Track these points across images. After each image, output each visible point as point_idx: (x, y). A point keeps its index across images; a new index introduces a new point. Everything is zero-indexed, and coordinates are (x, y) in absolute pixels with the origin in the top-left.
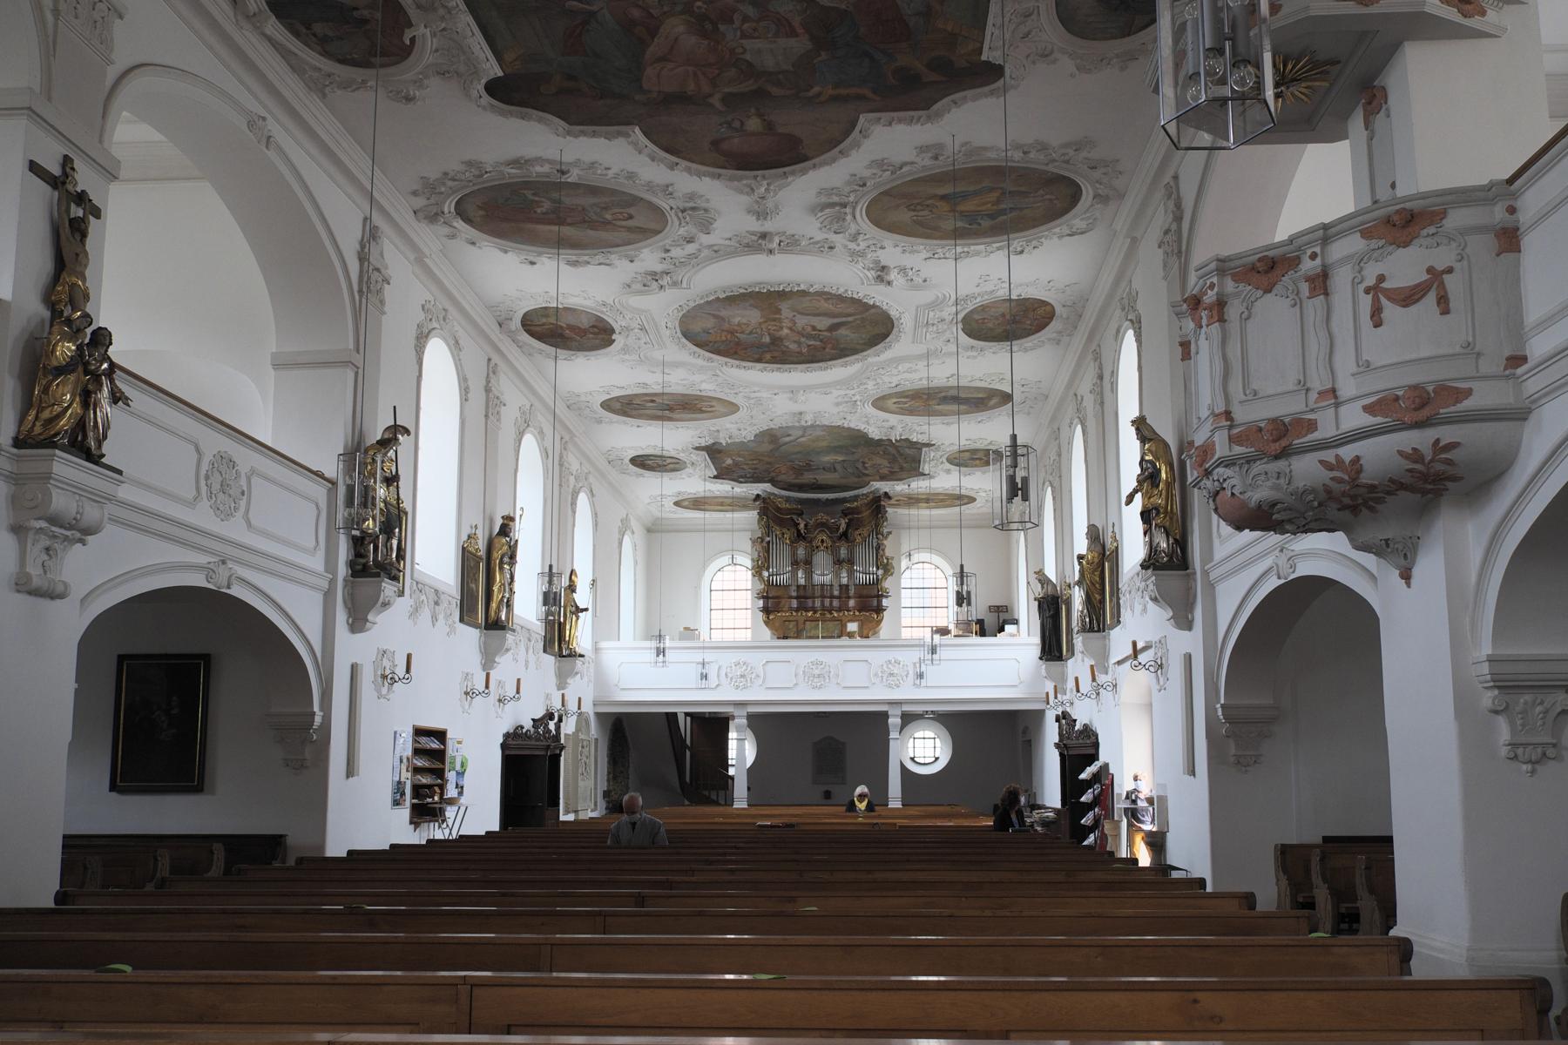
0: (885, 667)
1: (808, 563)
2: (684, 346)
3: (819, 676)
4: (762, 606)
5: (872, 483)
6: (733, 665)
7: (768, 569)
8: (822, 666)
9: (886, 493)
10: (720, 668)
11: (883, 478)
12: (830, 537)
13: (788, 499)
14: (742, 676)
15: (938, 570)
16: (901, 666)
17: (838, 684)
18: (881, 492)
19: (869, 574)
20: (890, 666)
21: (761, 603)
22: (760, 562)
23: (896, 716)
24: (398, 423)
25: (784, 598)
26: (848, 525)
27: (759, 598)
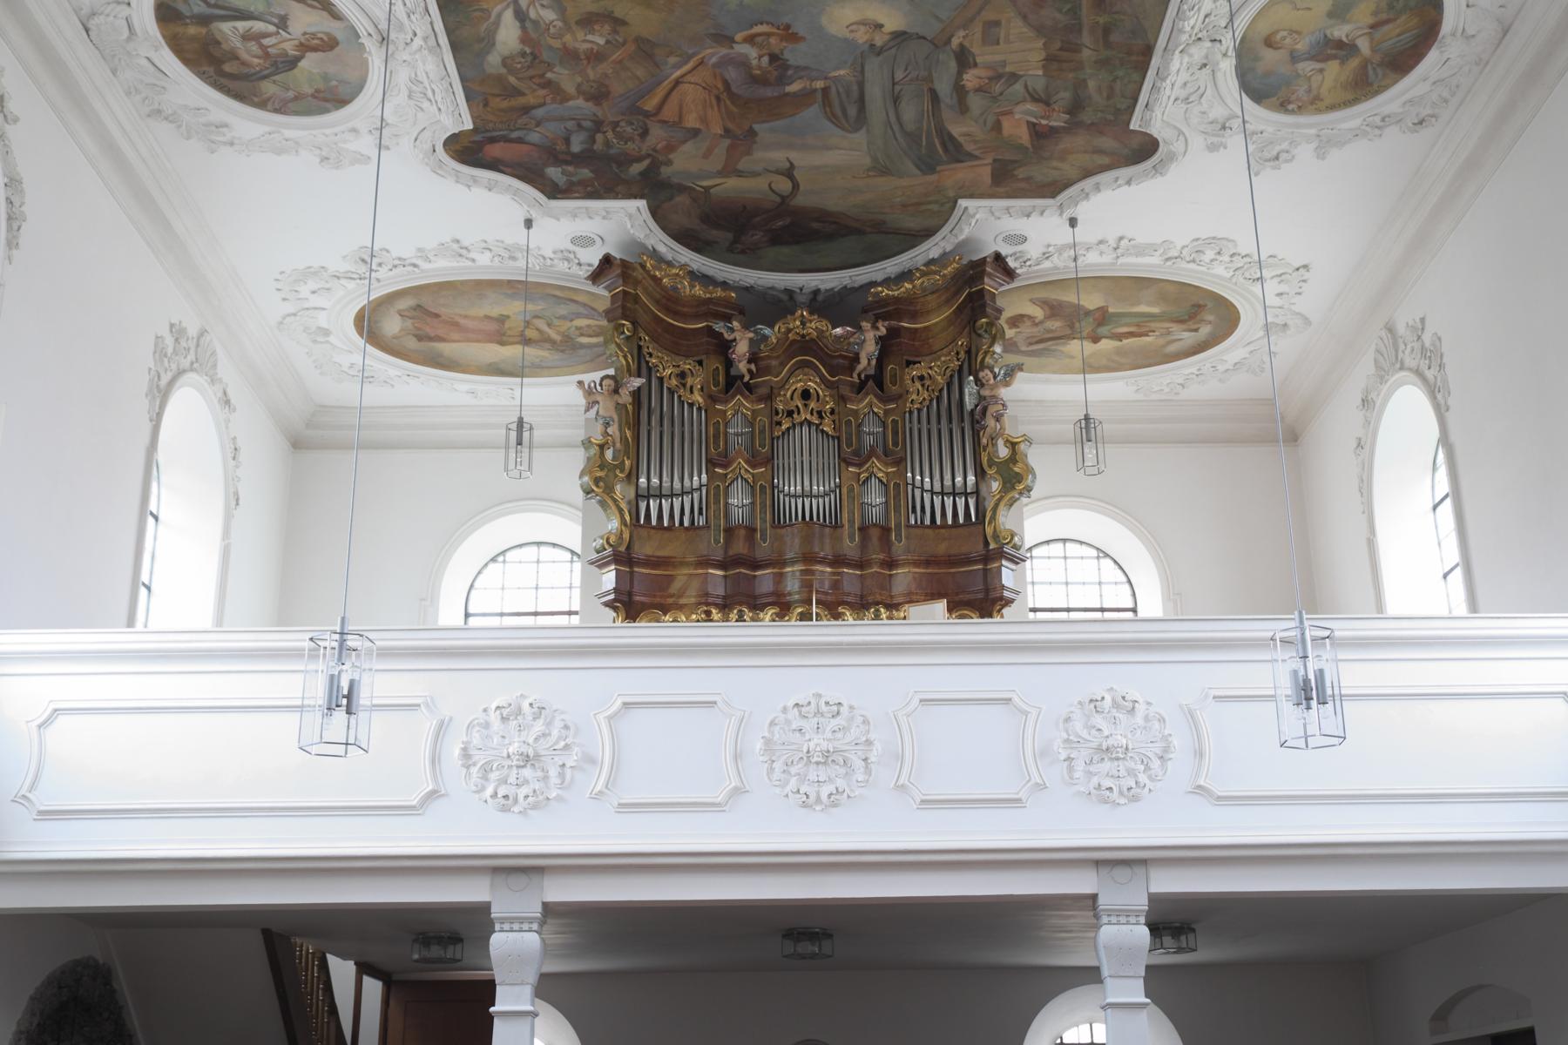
0: (1078, 725)
1: (764, 458)
2: (475, 180)
3: (828, 758)
6: (494, 718)
7: (632, 476)
8: (838, 721)
9: (998, 258)
10: (441, 728)
12: (829, 385)
13: (696, 277)
14: (527, 760)
15: (1107, 563)
16: (1139, 719)
17: (901, 788)
18: (988, 251)
19: (966, 494)
20: (1098, 720)
21: (609, 579)
22: (609, 454)
23: (1123, 914)
25: (683, 564)
27: (601, 564)
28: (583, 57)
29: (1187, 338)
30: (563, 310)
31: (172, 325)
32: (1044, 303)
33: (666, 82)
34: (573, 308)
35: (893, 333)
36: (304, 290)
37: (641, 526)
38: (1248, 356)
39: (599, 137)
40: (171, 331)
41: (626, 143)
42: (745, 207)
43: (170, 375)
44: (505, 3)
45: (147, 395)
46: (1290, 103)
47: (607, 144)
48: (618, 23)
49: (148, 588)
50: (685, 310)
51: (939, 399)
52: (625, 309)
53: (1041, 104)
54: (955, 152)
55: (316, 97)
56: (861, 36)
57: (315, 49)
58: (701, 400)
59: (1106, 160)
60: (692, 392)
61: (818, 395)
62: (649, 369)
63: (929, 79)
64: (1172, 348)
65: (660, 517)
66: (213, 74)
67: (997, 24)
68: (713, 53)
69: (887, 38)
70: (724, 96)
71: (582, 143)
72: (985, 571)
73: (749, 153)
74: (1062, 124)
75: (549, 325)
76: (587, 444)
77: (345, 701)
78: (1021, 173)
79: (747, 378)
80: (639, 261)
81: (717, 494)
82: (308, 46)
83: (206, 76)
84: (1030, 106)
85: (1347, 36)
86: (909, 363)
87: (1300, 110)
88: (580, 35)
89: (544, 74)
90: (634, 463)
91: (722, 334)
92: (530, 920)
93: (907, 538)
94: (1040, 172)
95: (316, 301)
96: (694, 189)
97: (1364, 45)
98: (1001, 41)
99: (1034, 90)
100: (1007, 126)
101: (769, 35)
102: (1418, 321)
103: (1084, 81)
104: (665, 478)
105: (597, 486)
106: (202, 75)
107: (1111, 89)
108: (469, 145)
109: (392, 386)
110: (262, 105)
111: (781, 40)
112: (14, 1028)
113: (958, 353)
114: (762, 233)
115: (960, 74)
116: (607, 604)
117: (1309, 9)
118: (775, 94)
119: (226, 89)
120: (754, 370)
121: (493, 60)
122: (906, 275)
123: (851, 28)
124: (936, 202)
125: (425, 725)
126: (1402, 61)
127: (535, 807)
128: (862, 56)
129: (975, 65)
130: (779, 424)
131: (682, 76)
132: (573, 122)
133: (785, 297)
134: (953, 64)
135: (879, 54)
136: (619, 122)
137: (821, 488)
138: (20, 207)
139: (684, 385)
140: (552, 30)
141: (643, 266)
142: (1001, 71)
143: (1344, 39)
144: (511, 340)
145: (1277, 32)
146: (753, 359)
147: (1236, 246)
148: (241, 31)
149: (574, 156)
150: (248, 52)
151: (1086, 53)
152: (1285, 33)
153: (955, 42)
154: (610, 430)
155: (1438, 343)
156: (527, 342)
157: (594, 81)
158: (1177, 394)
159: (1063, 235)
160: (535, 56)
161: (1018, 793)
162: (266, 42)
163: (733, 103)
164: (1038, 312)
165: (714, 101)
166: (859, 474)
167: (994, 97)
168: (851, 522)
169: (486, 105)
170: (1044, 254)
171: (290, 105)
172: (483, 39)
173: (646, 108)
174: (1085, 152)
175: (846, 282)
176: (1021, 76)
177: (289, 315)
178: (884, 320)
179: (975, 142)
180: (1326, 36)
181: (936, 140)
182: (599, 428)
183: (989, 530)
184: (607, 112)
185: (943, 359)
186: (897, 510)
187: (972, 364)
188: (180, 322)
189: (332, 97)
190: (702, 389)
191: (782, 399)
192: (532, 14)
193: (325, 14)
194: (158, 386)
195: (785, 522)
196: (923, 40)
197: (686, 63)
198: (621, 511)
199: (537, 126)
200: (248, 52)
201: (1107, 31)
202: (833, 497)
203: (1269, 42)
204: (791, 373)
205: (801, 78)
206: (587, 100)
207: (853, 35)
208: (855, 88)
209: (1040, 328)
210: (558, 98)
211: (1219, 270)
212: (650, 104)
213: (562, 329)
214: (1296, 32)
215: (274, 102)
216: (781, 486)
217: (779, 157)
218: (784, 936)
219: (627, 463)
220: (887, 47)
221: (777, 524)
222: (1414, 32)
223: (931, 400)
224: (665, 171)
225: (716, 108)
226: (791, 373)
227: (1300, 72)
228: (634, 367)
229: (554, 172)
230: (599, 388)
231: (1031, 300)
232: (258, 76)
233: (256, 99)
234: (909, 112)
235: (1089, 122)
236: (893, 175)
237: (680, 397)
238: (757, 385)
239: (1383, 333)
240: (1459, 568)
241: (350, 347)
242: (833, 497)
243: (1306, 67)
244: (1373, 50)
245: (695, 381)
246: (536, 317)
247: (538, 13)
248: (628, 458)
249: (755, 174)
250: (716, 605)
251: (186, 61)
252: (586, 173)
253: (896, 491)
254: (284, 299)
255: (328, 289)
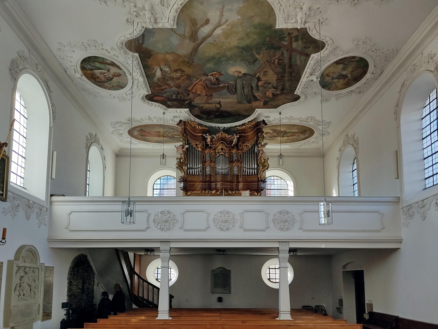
1: (213, 161)
4: (183, 186)
5: (256, 110)
11: (266, 105)
13: (199, 124)
14: (166, 221)
19: (255, 169)
21: (182, 185)
22: (182, 160)
24: (158, 278)
26: (239, 139)
27: (180, 182)
28: (175, 78)
29: (303, 137)
30: (171, 131)
31: (89, 133)
32: (273, 130)
33: (193, 84)
34: (174, 130)
35: (240, 136)
36: (117, 126)
37: (188, 175)
38: (315, 140)
39: (179, 96)
40: (89, 135)
41: (185, 97)
42: (210, 110)
43: (90, 144)
44: (158, 67)
45: (85, 148)
46: (331, 88)
47: (181, 97)
48: (183, 71)
49: (89, 185)
50: (197, 131)
51: (250, 150)
52: (185, 132)
53: (275, 89)
54: (256, 99)
55: (117, 87)
56: (236, 74)
57: (116, 76)
58: (200, 150)
59: (288, 101)
60: (199, 148)
61: (225, 149)
62: (190, 144)
63: (251, 84)
64: (299, 139)
65: (192, 173)
66: (94, 81)
67: (267, 71)
68: (204, 78)
69: (242, 75)
70: (206, 87)
71: (175, 97)
72: (258, 184)
73: (211, 99)
74: (280, 93)
75: (169, 133)
76: (177, 159)
77: (130, 214)
78: (270, 103)
79: (210, 146)
80: (187, 121)
81: (204, 168)
82: (114, 76)
83: (93, 81)
84: (273, 89)
85: (346, 74)
86: (244, 143)
87: (333, 90)
88: (174, 74)
89: (166, 82)
90: (187, 162)
91: (205, 137)
92: (168, 251)
93: (242, 177)
94: (273, 103)
95: (119, 128)
96: (199, 107)
97: (349, 76)
98: (267, 75)
99: (274, 86)
100: (267, 93)
101: (216, 74)
102: (354, 134)
103: (285, 84)
104: (193, 165)
105: (179, 167)
106: (92, 82)
107: (291, 85)
108: (151, 97)
109: (136, 145)
110: (105, 88)
111: (219, 75)
112: (69, 267)
113: (254, 141)
114: (213, 116)
115: (258, 82)
116: (181, 190)
117: (338, 68)
118: (217, 87)
119: (97, 85)
120: (211, 144)
121: (155, 79)
122: (244, 124)
123: (234, 73)
124: (251, 109)
125: (145, 215)
126: (357, 79)
127: (168, 230)
128: (236, 79)
129: (261, 81)
130: (217, 155)
131: (197, 83)
132: (173, 92)
133: (218, 128)
134: (256, 81)
135: (240, 78)
136: (183, 92)
137: (225, 167)
138: (55, 111)
139: (197, 147)
140: (168, 73)
141: (188, 122)
142: (267, 82)
143: (345, 74)
144: (161, 136)
145: (329, 73)
146: (211, 141)
147: (315, 118)
148: (100, 72)
149: (173, 99)
150: (102, 76)
151: (286, 78)
152: (331, 73)
153: (257, 76)
154: (182, 156)
155: (358, 139)
156: (164, 137)
157: (177, 84)
158: (299, 147)
159: (277, 116)
160: (164, 78)
161: (264, 229)
162: (105, 74)
163: (208, 89)
164: (271, 132)
165: (204, 88)
166: (233, 165)
167: (265, 88)
168: (231, 174)
169: (154, 89)
170: (273, 120)
171: (111, 88)
172: (153, 75)
173: (189, 90)
174: (284, 99)
175: (231, 126)
176: (271, 83)
177: (114, 131)
178: (239, 134)
179: (260, 97)
180: (341, 74)
181: (252, 97)
182: (180, 155)
183: (259, 176)
184: (181, 90)
185: (251, 142)
186: (240, 172)
187: (257, 143)
188: (91, 133)
189: (121, 87)
190: (201, 148)
191: (217, 150)
192: (164, 69)
193: (118, 68)
194: (87, 146)
195: (217, 174)
196: (250, 75)
197: (198, 80)
198: (184, 171)
199: (165, 93)
200: (102, 76)
201: (291, 73)
202: (227, 169)
203: (328, 75)
204: (219, 144)
205: (223, 83)
206: (176, 88)
207: (234, 74)
208: (234, 86)
209: (271, 134)
210: (170, 87)
211: (311, 123)
212: (190, 89)
213: (171, 134)
214: (334, 73)
215: (108, 88)
216: (217, 167)
217: (217, 100)
218: (217, 251)
219: (185, 162)
220: (242, 77)
221: (216, 175)
222: (361, 73)
223: (248, 150)
224: (193, 103)
225: (204, 90)
226: (219, 144)
227: (334, 82)
228: (187, 143)
229: (169, 103)
230: (179, 147)
231: (270, 129)
232: (104, 82)
233: (104, 87)
234: (246, 91)
235: (286, 93)
236: (242, 104)
237: (196, 149)
238: (212, 147)
239: (346, 136)
240: (357, 184)
241: (128, 138)
242: (227, 169)
243: (335, 81)
244: (351, 77)
245: (199, 146)
246: (166, 132)
247: (165, 69)
248: (186, 161)
249: (212, 104)
250: (204, 190)
251: (88, 79)
252: (176, 103)
253: (240, 169)
254: (113, 128)
255: (122, 126)
